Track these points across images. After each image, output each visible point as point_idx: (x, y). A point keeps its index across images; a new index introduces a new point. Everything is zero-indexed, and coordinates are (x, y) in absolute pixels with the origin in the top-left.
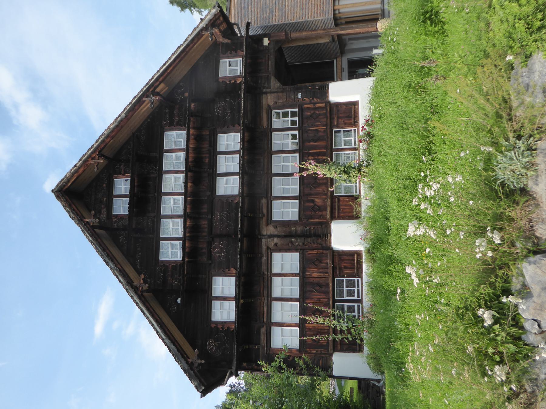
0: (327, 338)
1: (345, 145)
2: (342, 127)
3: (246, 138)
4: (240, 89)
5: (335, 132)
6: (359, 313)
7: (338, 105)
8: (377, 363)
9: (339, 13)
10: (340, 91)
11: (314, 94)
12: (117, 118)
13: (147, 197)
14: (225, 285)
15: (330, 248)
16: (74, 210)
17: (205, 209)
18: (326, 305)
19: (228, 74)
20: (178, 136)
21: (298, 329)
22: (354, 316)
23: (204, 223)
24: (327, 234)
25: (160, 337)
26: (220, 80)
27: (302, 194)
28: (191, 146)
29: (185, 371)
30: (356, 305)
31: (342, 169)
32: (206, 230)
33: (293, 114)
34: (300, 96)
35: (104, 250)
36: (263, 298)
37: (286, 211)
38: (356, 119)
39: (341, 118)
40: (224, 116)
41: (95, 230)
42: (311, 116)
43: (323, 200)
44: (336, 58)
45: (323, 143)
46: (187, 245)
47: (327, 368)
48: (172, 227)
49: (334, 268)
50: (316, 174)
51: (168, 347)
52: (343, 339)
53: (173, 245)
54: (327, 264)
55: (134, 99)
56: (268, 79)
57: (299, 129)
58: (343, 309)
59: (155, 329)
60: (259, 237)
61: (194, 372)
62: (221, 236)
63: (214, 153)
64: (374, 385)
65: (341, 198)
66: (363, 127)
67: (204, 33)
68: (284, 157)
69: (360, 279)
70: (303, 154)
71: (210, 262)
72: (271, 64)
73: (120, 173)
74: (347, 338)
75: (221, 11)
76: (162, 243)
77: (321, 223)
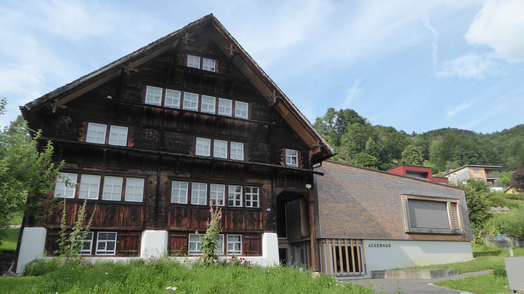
0: (63, 223)
1: (229, 244)
2: (243, 242)
3: (239, 165)
4: (276, 164)
5: (239, 237)
6: (83, 253)
7: (260, 239)
8: (36, 270)
9: (323, 243)
10: (270, 241)
11: (269, 221)
12: (262, 70)
13: (199, 83)
14: (119, 136)
15: (144, 229)
16: (196, 27)
17: (186, 127)
18: (93, 223)
19: (287, 155)
20: (244, 113)
21: (73, 197)
22: (80, 248)
23: (174, 125)
24: (157, 227)
25: (81, 78)
26: (283, 150)
27: (192, 207)
28: (236, 121)
29: (47, 95)
30: (90, 250)
31: (212, 241)
32: (169, 126)
33: (255, 204)
34: (269, 210)
35: (161, 44)
36: (105, 168)
37: (179, 193)
38: (249, 254)
39: (250, 242)
40: (257, 150)
41: (178, 40)
42: (253, 218)
43: (186, 225)
44: (288, 239)
45: (232, 226)
46: (157, 109)
47: (30, 221)
48: (173, 99)
49: (126, 231)
50: (210, 221)
51: (71, 84)
52: (60, 237)
53: (158, 98)
54: (131, 226)
55: (275, 84)
56: (282, 186)
57: (244, 207)
58: (87, 239)
59: (89, 75)
60: (159, 169)
61: (45, 103)
62: (162, 138)
63: (230, 139)
64: (9, 266)
65: (186, 239)
66: (244, 259)
67: (318, 141)
68: (222, 194)
69: (114, 254)
70: (225, 210)
71: (141, 127)
72: (292, 189)
73: (219, 65)
74: (60, 242)
75: (332, 155)
76: (161, 90)
77: (166, 222)
